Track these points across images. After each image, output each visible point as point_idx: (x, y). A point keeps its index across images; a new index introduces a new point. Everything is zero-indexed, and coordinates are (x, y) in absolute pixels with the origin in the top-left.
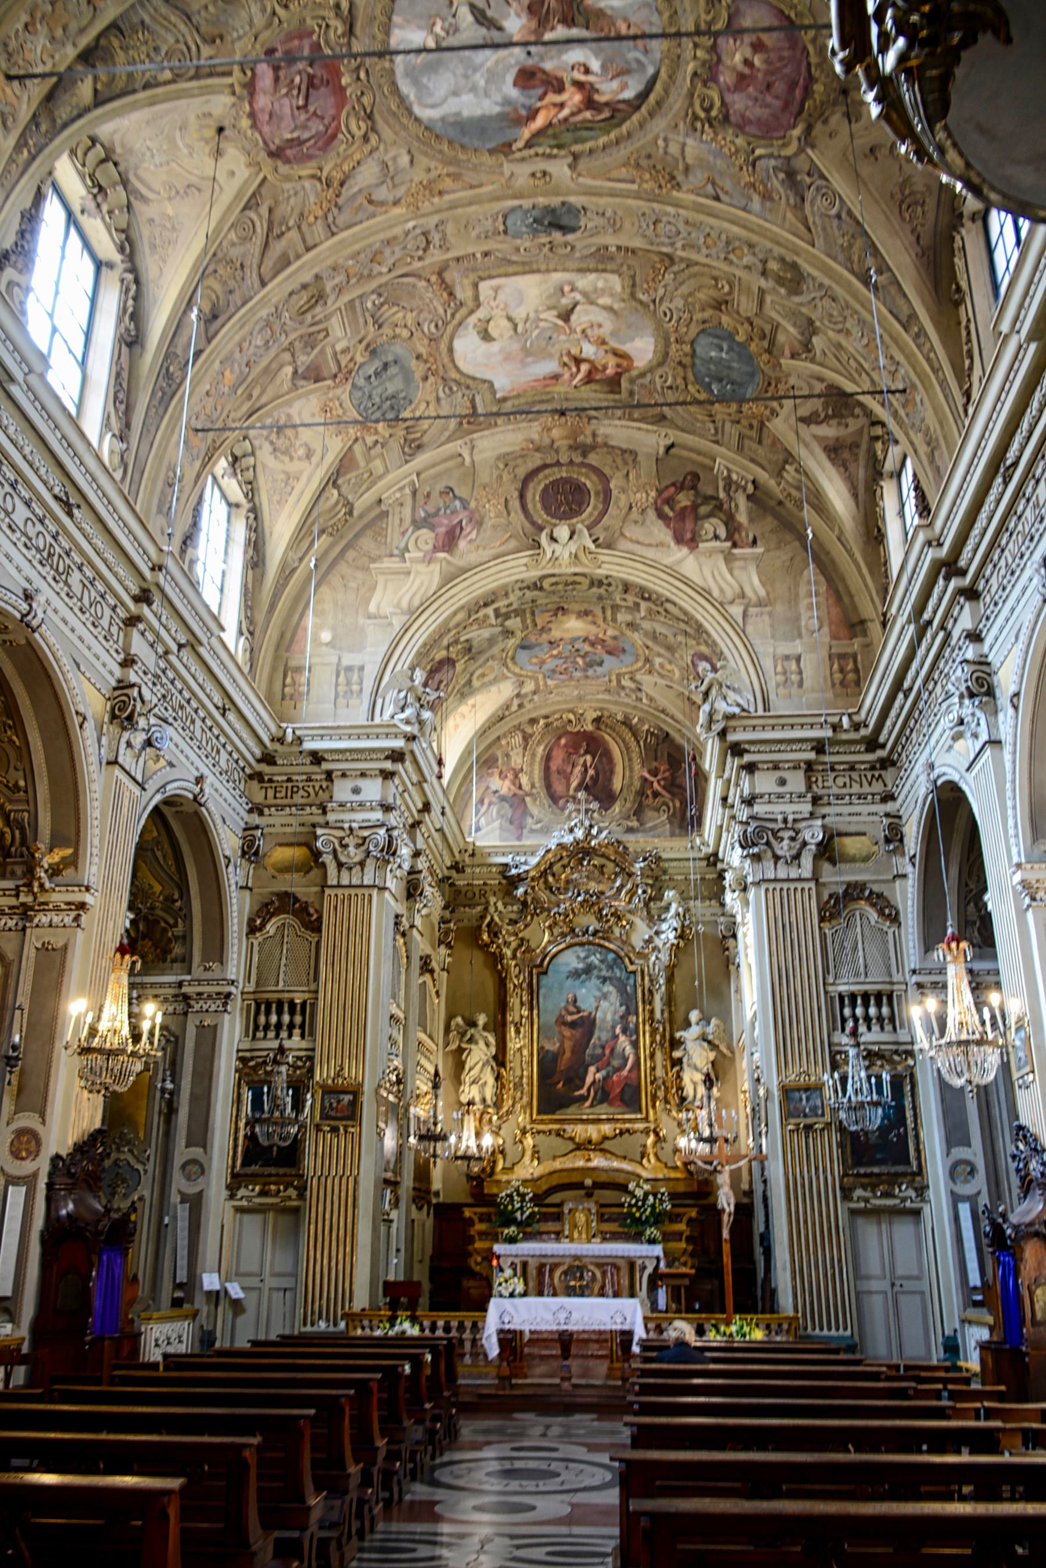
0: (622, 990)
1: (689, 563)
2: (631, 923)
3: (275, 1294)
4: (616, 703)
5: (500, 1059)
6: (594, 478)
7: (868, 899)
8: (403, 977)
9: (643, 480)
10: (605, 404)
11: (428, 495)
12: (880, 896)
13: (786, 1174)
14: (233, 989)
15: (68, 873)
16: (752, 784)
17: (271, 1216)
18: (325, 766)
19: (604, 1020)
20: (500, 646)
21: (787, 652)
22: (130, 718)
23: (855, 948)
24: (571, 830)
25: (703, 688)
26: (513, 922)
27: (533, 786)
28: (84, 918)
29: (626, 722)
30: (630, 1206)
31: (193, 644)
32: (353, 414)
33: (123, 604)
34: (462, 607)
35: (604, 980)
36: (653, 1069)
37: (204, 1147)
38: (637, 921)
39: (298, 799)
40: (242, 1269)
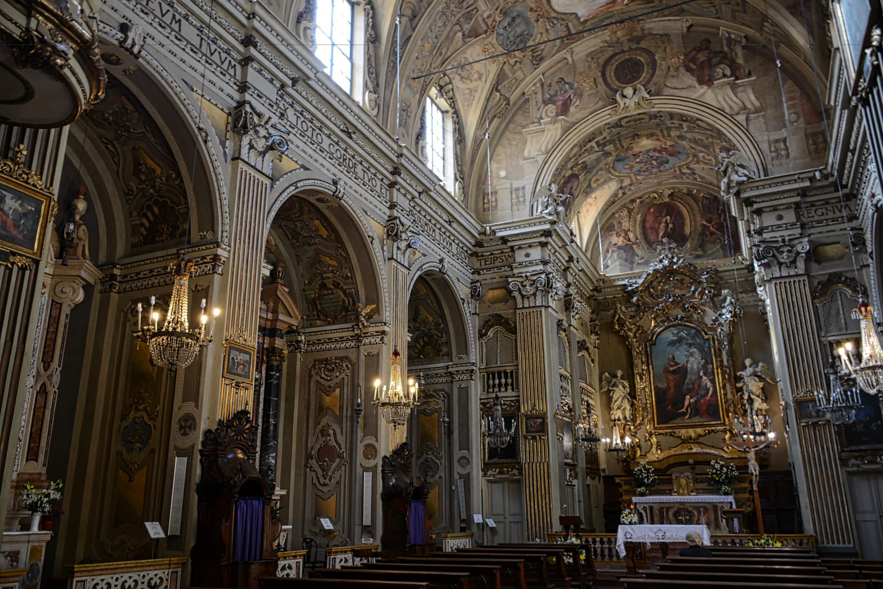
0: (701, 351)
1: (709, 95)
2: (704, 311)
3: (512, 525)
4: (681, 183)
5: (632, 395)
6: (645, 55)
7: (844, 283)
8: (568, 354)
9: (676, 50)
10: (646, 11)
11: (550, 85)
12: (853, 279)
13: (802, 452)
14: (474, 368)
15: (375, 317)
16: (761, 222)
17: (506, 484)
18: (509, 244)
19: (692, 368)
20: (604, 162)
21: (777, 138)
22: (396, 235)
23: (839, 313)
24: (661, 261)
25: (723, 169)
26: (632, 317)
27: (637, 238)
28: (385, 338)
29: (689, 193)
30: (713, 474)
31: (426, 191)
32: (500, 50)
33: (386, 177)
34: (576, 145)
35: (690, 345)
36: (725, 394)
37: (468, 450)
38: (707, 309)
39: (497, 264)
40: (494, 512)
